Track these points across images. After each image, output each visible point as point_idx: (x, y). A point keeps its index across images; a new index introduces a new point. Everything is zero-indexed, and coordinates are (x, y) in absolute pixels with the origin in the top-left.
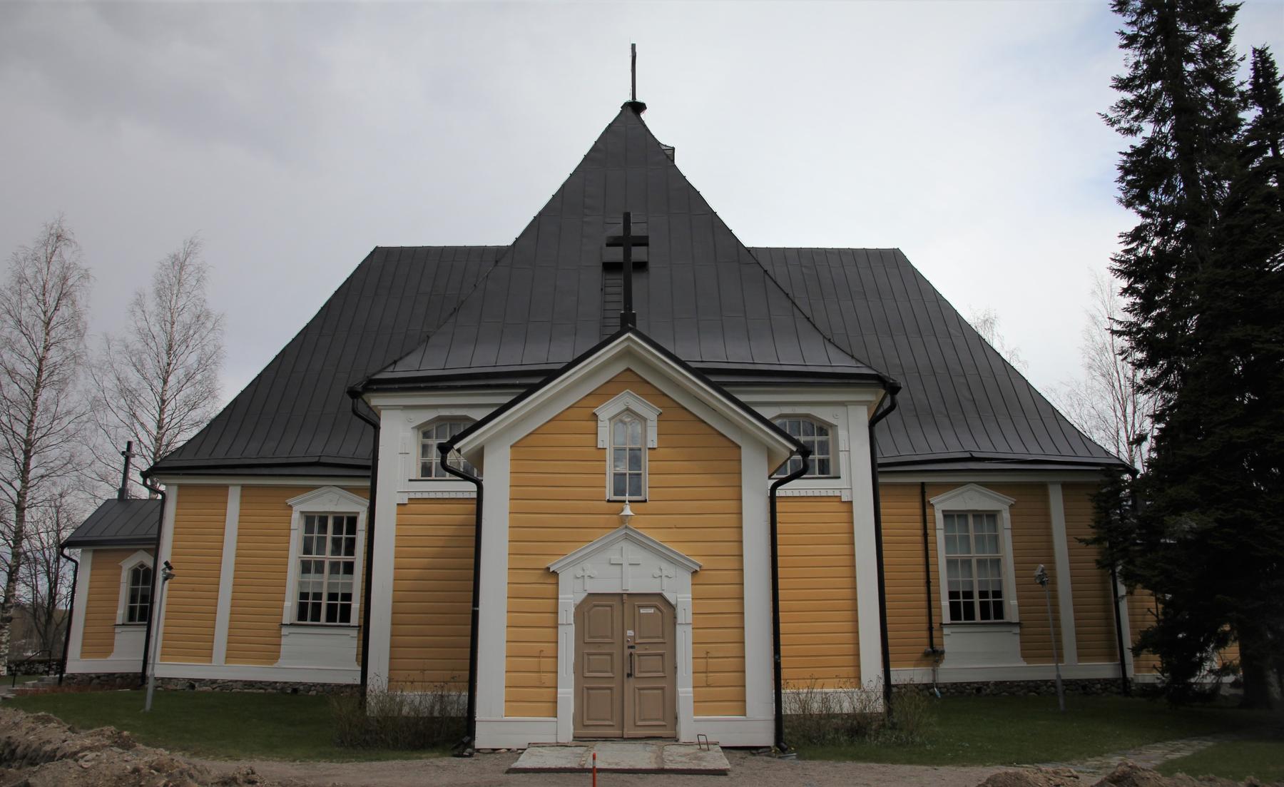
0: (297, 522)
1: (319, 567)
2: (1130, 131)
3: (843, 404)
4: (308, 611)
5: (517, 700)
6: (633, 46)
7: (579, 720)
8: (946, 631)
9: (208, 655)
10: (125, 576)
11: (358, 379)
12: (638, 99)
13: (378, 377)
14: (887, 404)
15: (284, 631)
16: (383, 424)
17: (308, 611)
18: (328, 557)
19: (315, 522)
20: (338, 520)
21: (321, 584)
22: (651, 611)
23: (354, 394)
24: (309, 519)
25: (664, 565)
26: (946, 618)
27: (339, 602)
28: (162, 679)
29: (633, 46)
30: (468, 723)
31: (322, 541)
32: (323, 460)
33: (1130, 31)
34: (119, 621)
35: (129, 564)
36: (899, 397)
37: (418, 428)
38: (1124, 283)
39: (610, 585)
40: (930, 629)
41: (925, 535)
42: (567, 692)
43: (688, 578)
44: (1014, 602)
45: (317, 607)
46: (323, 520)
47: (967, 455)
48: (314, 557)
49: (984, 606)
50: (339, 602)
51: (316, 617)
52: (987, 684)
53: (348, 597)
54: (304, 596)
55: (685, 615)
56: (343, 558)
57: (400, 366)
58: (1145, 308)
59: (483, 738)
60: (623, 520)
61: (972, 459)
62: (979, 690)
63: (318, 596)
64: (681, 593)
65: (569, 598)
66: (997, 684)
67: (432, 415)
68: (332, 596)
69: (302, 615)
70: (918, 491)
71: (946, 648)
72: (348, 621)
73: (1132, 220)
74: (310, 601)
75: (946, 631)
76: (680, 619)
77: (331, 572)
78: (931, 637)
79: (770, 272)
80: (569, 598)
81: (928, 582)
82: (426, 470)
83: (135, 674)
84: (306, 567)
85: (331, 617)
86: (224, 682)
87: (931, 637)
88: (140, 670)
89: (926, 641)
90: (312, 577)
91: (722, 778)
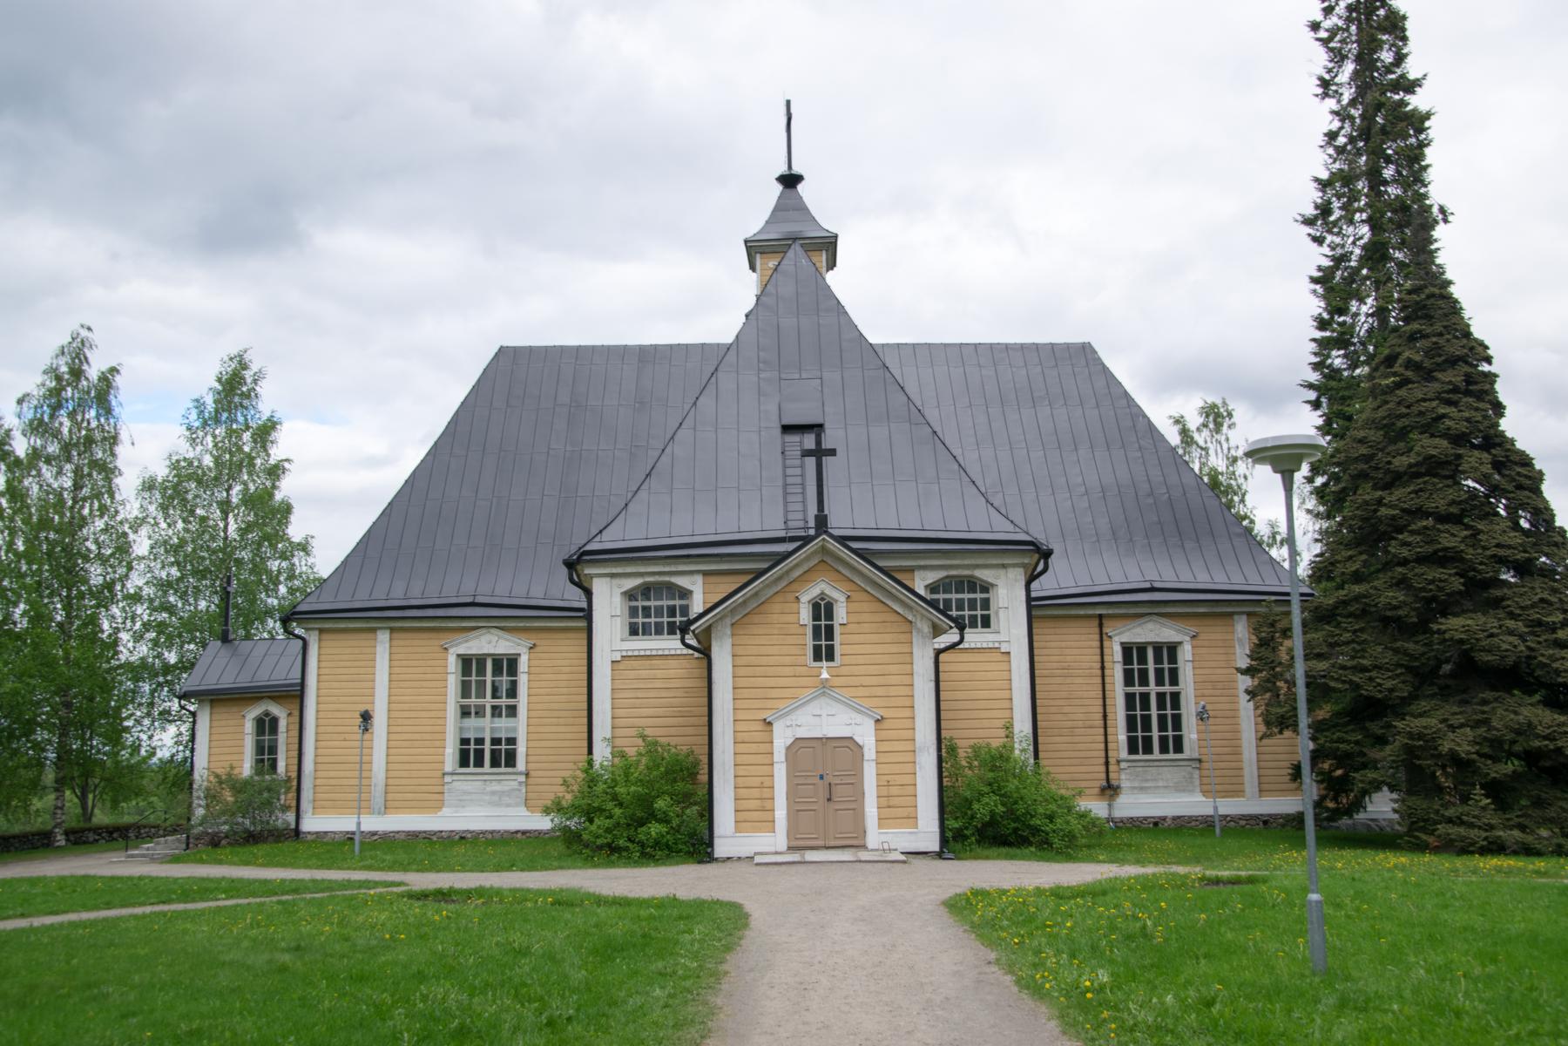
0: (453, 664)
1: (480, 713)
3: (1004, 566)
4: (470, 755)
5: (743, 823)
6: (788, 103)
7: (792, 832)
10: (249, 726)
11: (570, 550)
12: (796, 169)
13: (588, 548)
14: (1040, 567)
15: (448, 779)
16: (594, 591)
17: (470, 755)
18: (488, 701)
19: (466, 661)
21: (483, 729)
23: (570, 565)
24: (466, 661)
25: (854, 714)
26: (1124, 754)
27: (503, 747)
29: (788, 103)
31: (481, 685)
32: (479, 599)
35: (254, 712)
36: (1053, 560)
37: (624, 594)
39: (803, 733)
41: (1103, 668)
42: (781, 813)
43: (871, 723)
44: (1194, 736)
47: (1148, 585)
50: (503, 747)
52: (1164, 819)
54: (465, 741)
55: (870, 753)
56: (504, 701)
57: (606, 535)
59: (721, 848)
60: (824, 685)
61: (1152, 589)
62: (1156, 824)
63: (480, 741)
64: (865, 734)
65: (782, 738)
66: (1175, 818)
69: (464, 762)
70: (1096, 622)
74: (472, 747)
75: (1123, 765)
76: (866, 757)
77: (493, 715)
78: (1107, 772)
80: (782, 738)
82: (634, 631)
84: (465, 712)
85: (495, 763)
87: (1107, 772)
89: (1103, 776)
90: (472, 722)
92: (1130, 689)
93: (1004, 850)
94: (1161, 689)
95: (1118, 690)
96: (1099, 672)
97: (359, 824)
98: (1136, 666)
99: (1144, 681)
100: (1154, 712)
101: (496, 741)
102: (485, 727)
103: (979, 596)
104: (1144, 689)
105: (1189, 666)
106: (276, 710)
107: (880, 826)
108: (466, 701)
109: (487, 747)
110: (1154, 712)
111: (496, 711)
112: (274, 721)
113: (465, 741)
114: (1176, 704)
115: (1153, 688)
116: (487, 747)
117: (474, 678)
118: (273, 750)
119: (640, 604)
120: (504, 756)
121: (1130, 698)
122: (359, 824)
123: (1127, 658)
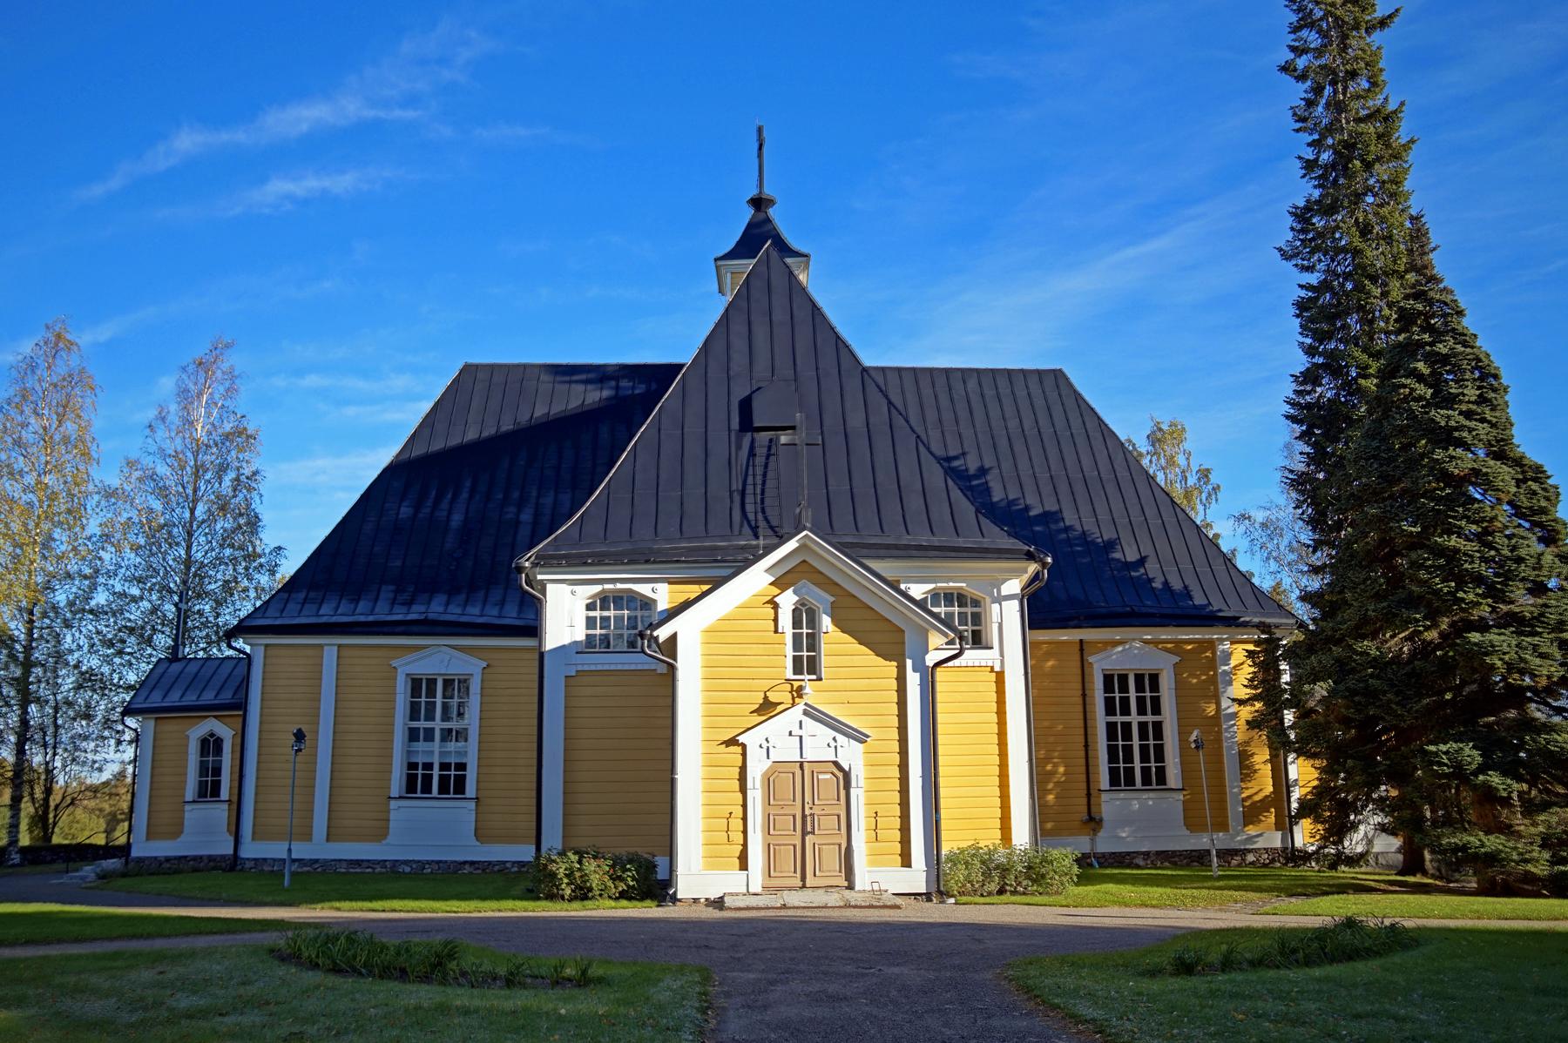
2: (1309, 269)
4: (417, 782)
8: (1104, 797)
9: (307, 836)
12: (768, 191)
17: (417, 782)
20: (448, 683)
22: (828, 776)
28: (255, 860)
29: (760, 130)
30: (669, 882)
31: (431, 707)
33: (1309, 154)
34: (189, 797)
38: (1298, 429)
40: (1089, 795)
45: (428, 779)
46: (432, 683)
48: (422, 724)
49: (444, 781)
51: (427, 788)
53: (462, 767)
54: (412, 766)
58: (1318, 458)
63: (428, 766)
65: (757, 768)
67: (597, 588)
68: (445, 766)
69: (411, 786)
71: (1104, 815)
72: (218, 795)
73: (1301, 362)
74: (420, 772)
79: (924, 437)
81: (1086, 746)
83: (223, 857)
84: (413, 735)
86: (326, 861)
88: (231, 852)
89: (1085, 809)
90: (421, 746)
91: (765, 134)
92: (1112, 719)
93: (39, 868)
94: (1143, 719)
95: (1100, 719)
96: (1080, 700)
97: (290, 850)
98: (1117, 695)
99: (1126, 711)
100: (1136, 742)
101: (445, 766)
102: (433, 752)
103: (969, 610)
104: (1143, 719)
105: (861, 792)
106: (212, 725)
107: (872, 864)
108: (415, 724)
109: (436, 773)
110: (1136, 742)
111: (447, 734)
112: (218, 743)
113: (412, 766)
114: (1159, 734)
115: (1134, 719)
116: (436, 773)
117: (423, 699)
118: (217, 771)
119: (597, 614)
120: (453, 784)
121: (1111, 727)
122: (290, 850)
123: (1108, 687)
